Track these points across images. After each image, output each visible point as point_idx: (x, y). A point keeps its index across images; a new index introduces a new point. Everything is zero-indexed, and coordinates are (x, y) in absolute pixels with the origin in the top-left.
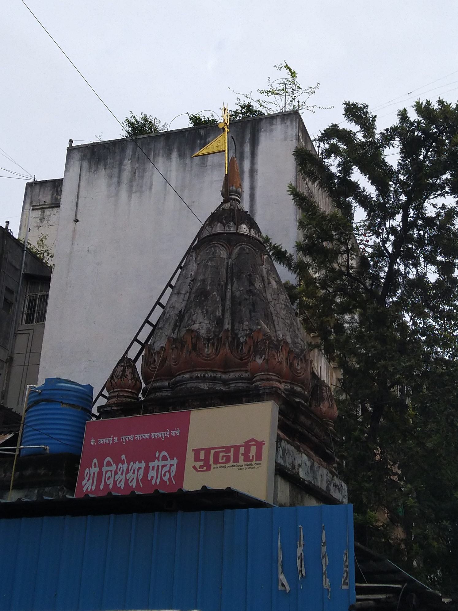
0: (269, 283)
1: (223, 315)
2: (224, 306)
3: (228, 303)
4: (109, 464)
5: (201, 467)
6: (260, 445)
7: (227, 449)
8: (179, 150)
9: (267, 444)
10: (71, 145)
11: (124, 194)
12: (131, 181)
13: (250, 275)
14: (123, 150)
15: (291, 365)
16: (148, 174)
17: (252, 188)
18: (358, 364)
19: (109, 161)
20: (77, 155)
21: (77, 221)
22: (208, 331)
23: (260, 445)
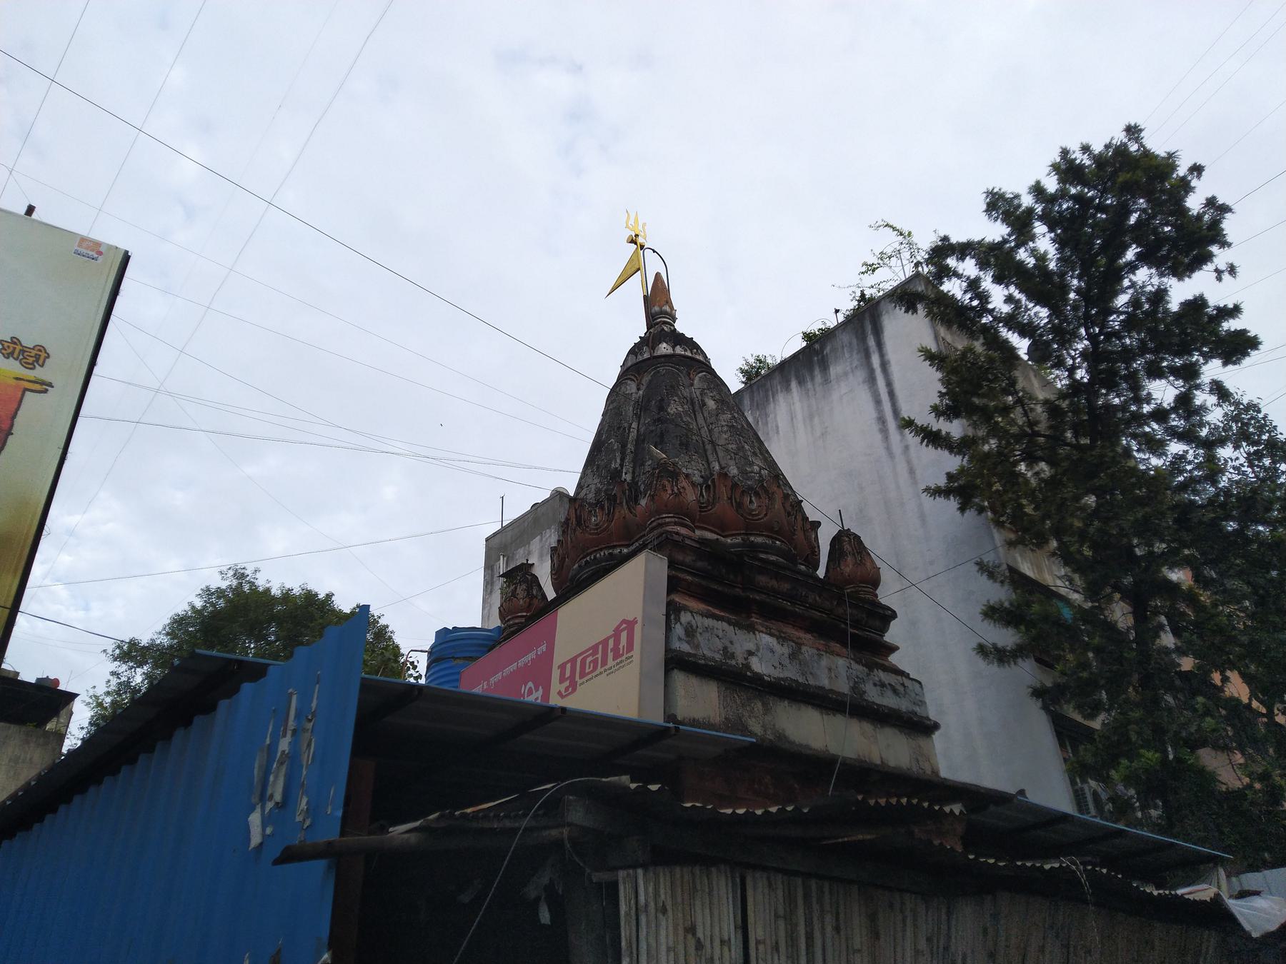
0: (704, 404)
1: (622, 465)
3: (630, 447)
5: (567, 689)
7: (595, 649)
8: (797, 378)
13: (662, 400)
17: (889, 384)
18: (1047, 542)
22: (598, 491)
23: (630, 625)
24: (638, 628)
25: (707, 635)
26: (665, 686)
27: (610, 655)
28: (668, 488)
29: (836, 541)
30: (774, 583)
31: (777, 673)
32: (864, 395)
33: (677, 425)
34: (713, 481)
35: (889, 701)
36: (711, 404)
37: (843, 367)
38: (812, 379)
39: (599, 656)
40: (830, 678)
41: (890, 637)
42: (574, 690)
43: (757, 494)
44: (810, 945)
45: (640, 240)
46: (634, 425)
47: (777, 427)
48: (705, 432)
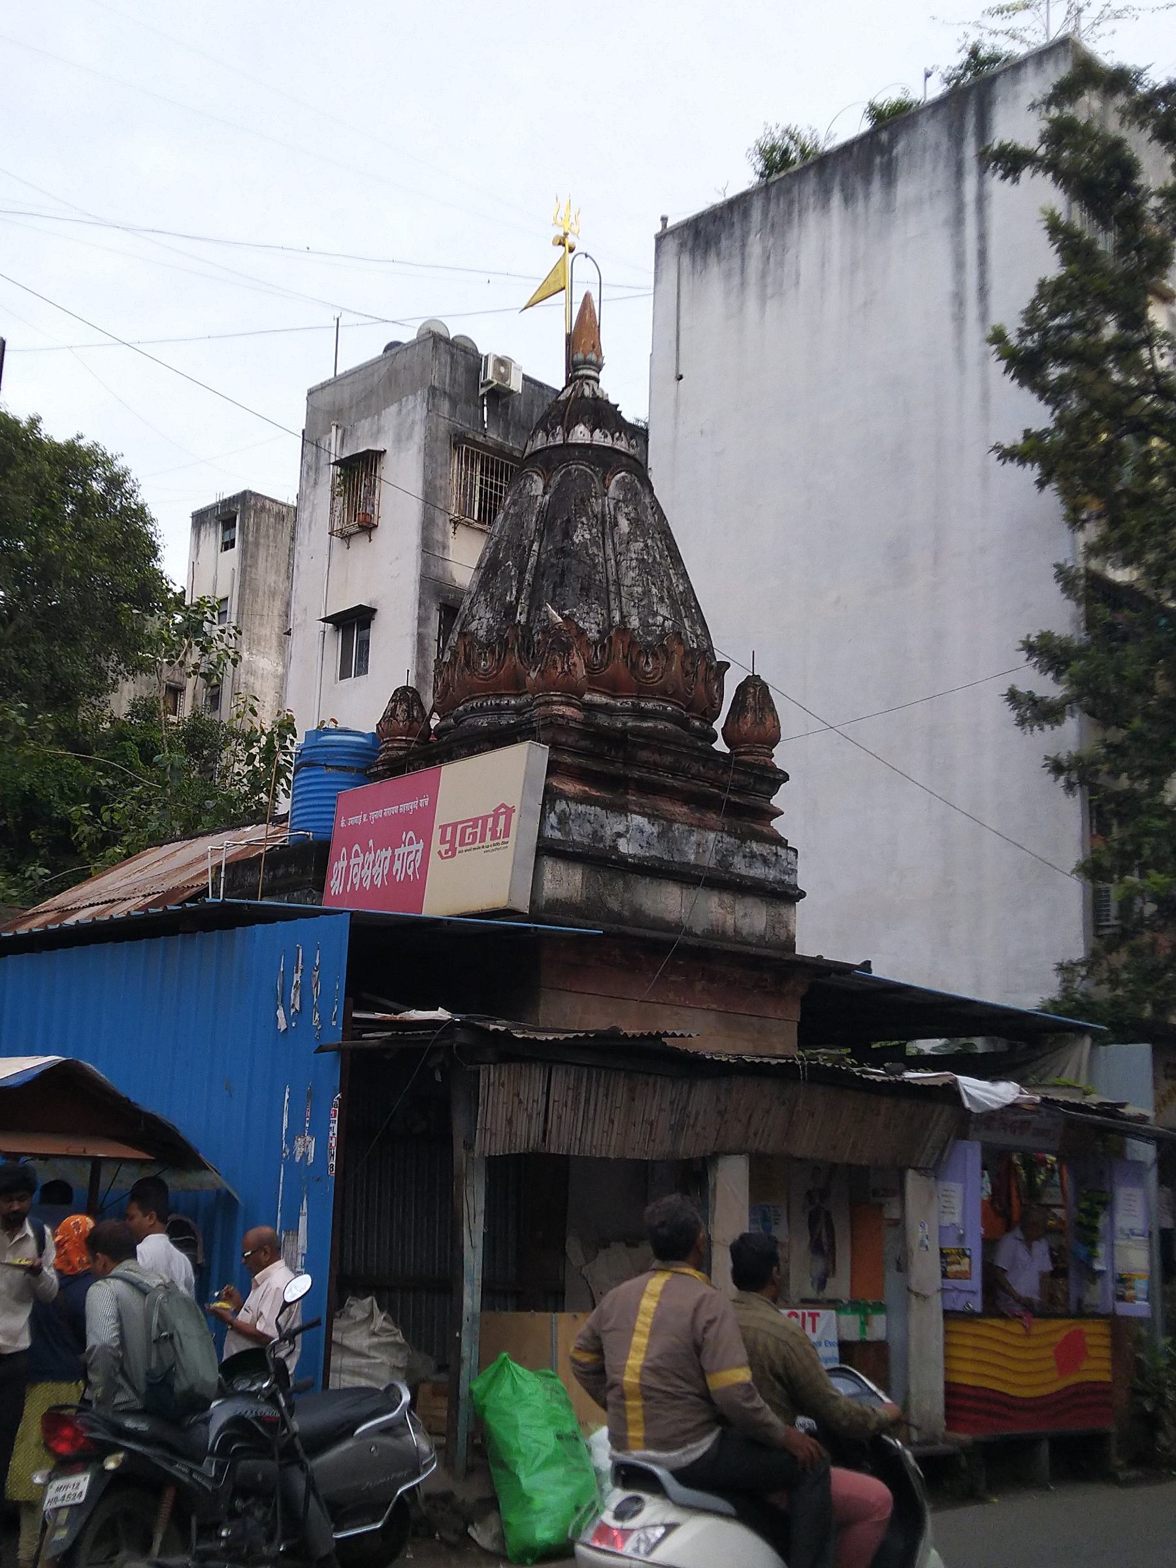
0: (616, 524)
1: (517, 599)
2: (520, 582)
4: (356, 855)
5: (446, 852)
6: (509, 811)
7: (476, 820)
9: (517, 809)
10: (665, 226)
11: (752, 305)
12: (764, 275)
13: (569, 520)
14: (746, 215)
15: (635, 666)
16: (790, 255)
17: (982, 237)
19: (724, 243)
20: (671, 245)
21: (680, 378)
22: (490, 629)
23: (509, 811)
24: (515, 816)
25: (578, 822)
26: (656, 273)
27: (489, 834)
28: (559, 666)
29: (742, 689)
30: (657, 757)
31: (641, 853)
32: (940, 249)
33: (580, 561)
34: (610, 639)
35: (758, 871)
36: (624, 525)
37: (920, 182)
38: (867, 197)
39: (479, 830)
40: (697, 853)
41: (776, 801)
42: (454, 855)
43: (655, 655)
44: (587, 1101)
45: (569, 241)
46: (535, 547)
47: (798, 275)
48: (612, 570)
